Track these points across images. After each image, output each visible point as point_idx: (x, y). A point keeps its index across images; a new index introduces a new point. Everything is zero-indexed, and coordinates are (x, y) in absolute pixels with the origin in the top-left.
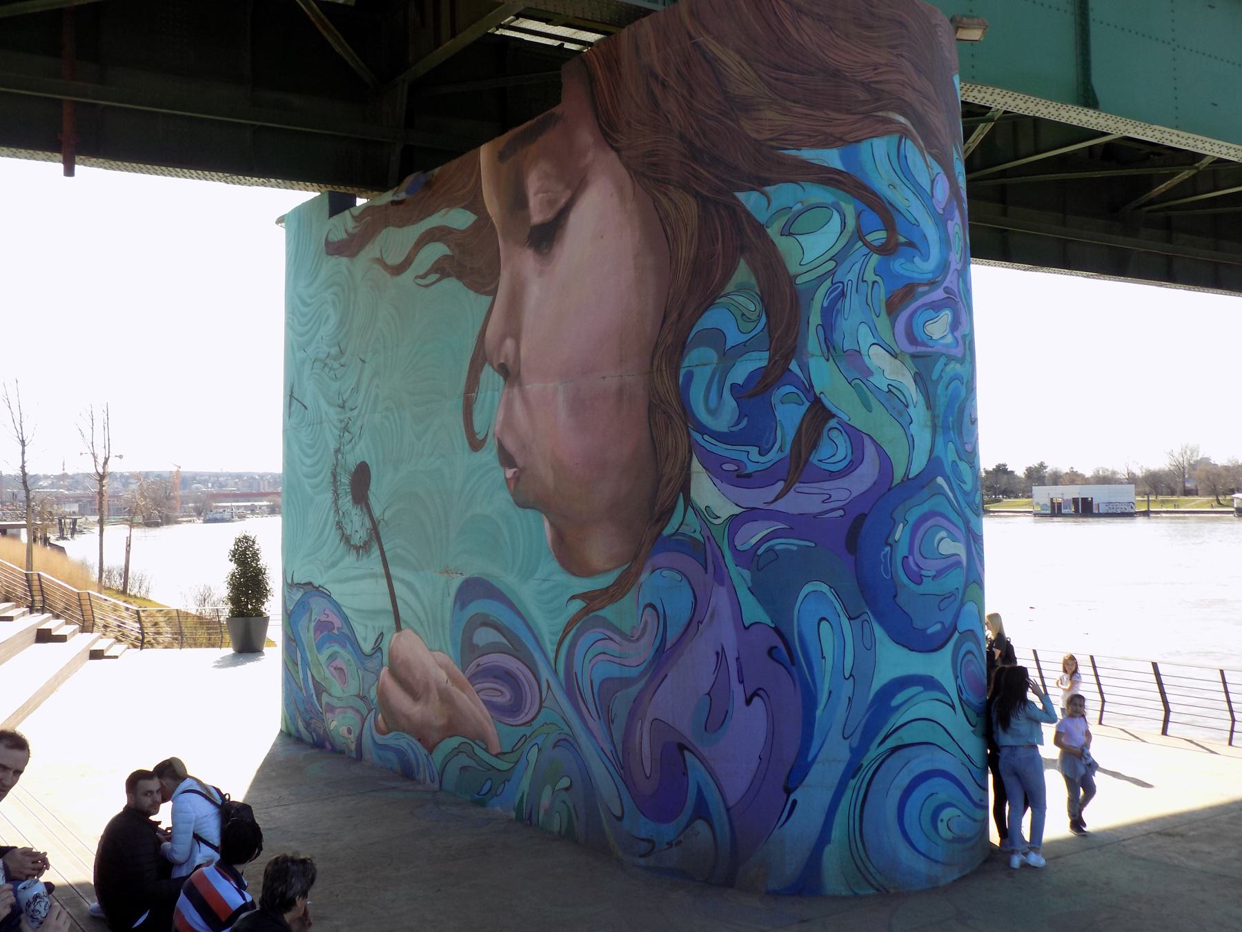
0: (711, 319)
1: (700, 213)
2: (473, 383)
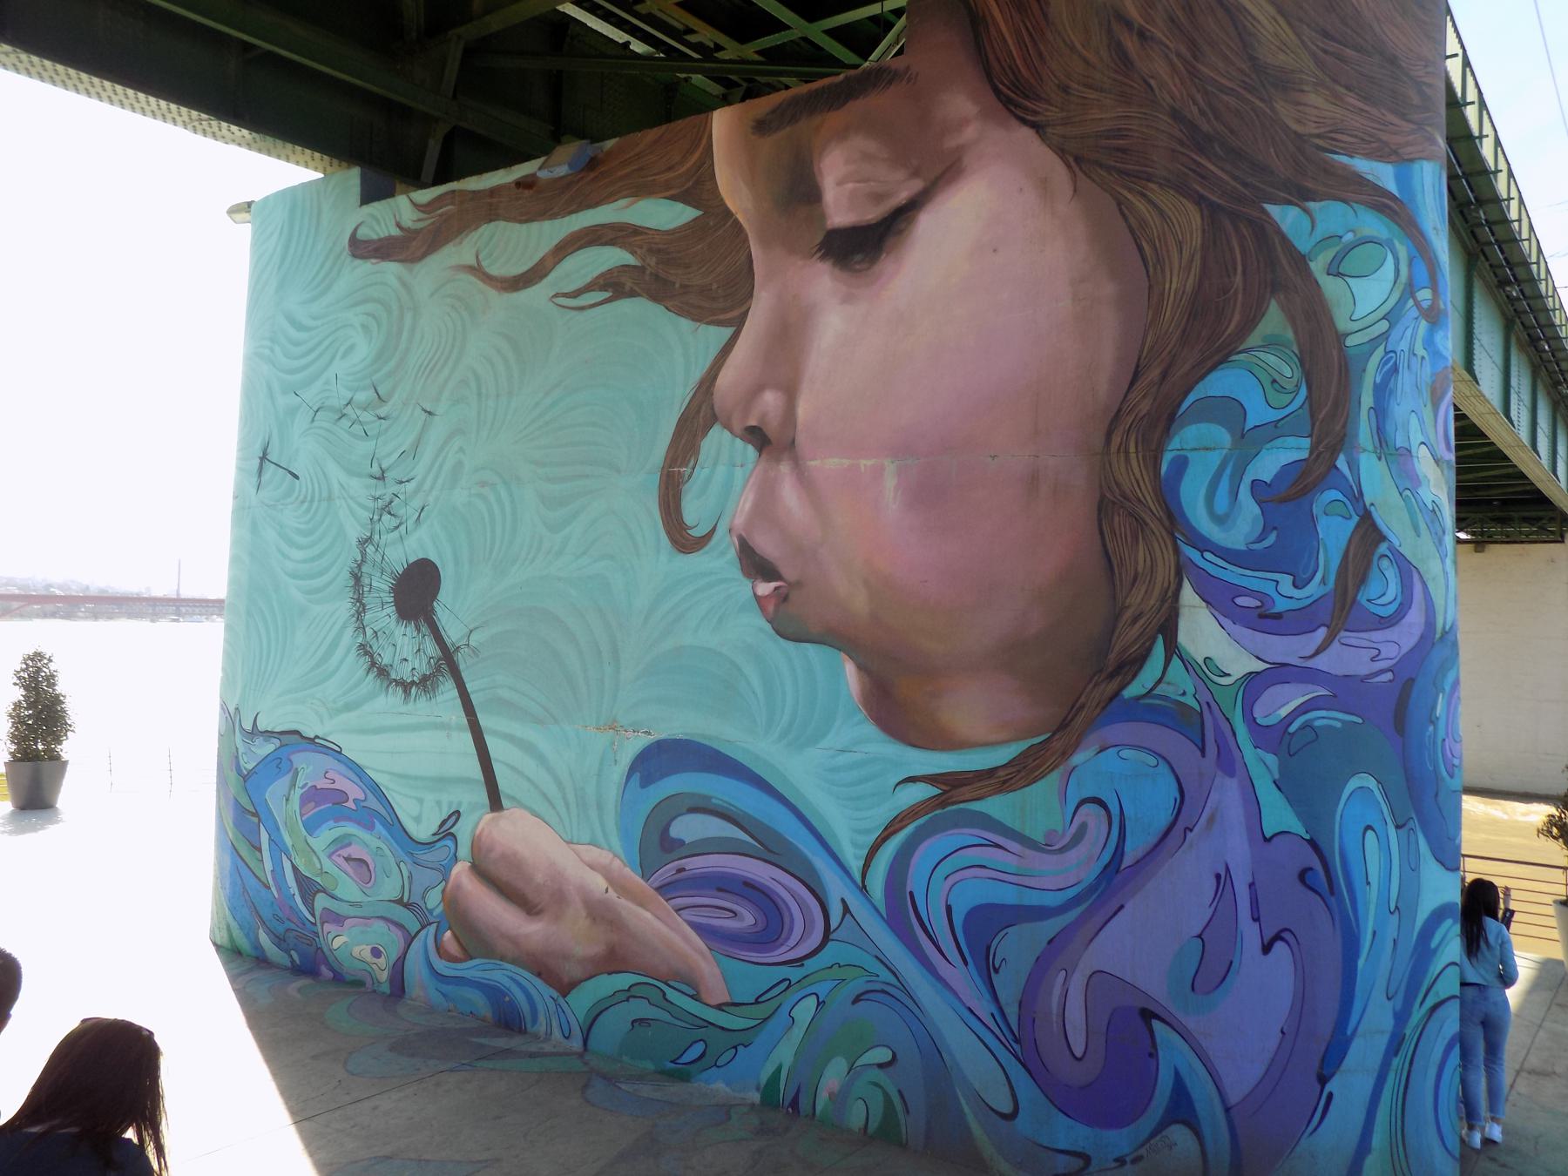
0: (1220, 383)
1: (1206, 228)
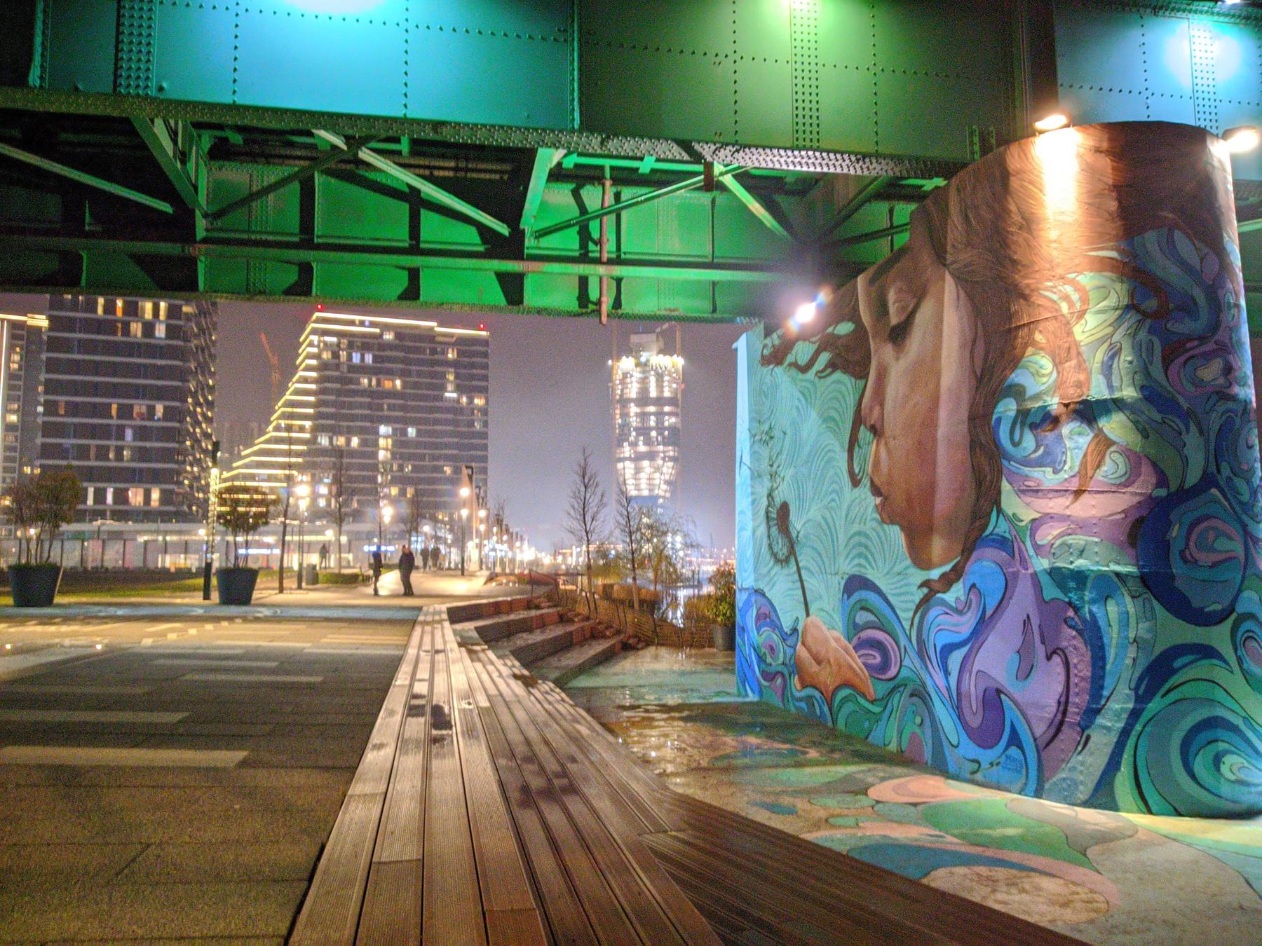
2: (853, 441)
